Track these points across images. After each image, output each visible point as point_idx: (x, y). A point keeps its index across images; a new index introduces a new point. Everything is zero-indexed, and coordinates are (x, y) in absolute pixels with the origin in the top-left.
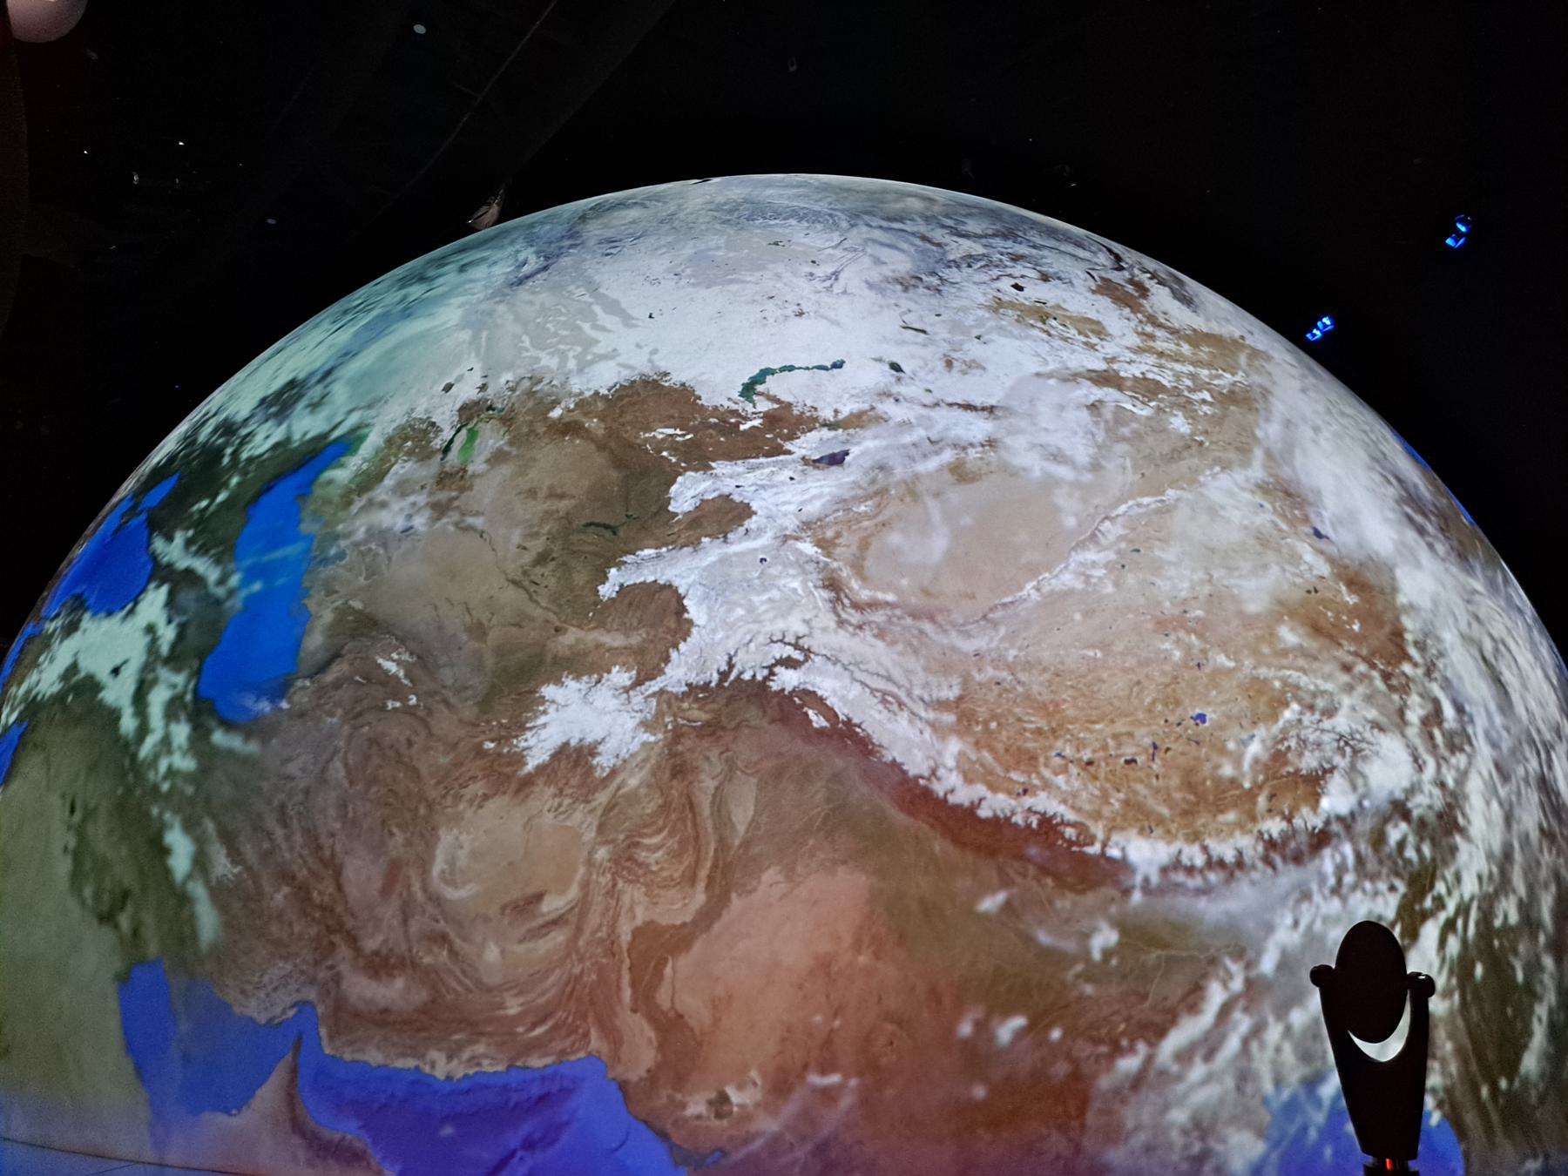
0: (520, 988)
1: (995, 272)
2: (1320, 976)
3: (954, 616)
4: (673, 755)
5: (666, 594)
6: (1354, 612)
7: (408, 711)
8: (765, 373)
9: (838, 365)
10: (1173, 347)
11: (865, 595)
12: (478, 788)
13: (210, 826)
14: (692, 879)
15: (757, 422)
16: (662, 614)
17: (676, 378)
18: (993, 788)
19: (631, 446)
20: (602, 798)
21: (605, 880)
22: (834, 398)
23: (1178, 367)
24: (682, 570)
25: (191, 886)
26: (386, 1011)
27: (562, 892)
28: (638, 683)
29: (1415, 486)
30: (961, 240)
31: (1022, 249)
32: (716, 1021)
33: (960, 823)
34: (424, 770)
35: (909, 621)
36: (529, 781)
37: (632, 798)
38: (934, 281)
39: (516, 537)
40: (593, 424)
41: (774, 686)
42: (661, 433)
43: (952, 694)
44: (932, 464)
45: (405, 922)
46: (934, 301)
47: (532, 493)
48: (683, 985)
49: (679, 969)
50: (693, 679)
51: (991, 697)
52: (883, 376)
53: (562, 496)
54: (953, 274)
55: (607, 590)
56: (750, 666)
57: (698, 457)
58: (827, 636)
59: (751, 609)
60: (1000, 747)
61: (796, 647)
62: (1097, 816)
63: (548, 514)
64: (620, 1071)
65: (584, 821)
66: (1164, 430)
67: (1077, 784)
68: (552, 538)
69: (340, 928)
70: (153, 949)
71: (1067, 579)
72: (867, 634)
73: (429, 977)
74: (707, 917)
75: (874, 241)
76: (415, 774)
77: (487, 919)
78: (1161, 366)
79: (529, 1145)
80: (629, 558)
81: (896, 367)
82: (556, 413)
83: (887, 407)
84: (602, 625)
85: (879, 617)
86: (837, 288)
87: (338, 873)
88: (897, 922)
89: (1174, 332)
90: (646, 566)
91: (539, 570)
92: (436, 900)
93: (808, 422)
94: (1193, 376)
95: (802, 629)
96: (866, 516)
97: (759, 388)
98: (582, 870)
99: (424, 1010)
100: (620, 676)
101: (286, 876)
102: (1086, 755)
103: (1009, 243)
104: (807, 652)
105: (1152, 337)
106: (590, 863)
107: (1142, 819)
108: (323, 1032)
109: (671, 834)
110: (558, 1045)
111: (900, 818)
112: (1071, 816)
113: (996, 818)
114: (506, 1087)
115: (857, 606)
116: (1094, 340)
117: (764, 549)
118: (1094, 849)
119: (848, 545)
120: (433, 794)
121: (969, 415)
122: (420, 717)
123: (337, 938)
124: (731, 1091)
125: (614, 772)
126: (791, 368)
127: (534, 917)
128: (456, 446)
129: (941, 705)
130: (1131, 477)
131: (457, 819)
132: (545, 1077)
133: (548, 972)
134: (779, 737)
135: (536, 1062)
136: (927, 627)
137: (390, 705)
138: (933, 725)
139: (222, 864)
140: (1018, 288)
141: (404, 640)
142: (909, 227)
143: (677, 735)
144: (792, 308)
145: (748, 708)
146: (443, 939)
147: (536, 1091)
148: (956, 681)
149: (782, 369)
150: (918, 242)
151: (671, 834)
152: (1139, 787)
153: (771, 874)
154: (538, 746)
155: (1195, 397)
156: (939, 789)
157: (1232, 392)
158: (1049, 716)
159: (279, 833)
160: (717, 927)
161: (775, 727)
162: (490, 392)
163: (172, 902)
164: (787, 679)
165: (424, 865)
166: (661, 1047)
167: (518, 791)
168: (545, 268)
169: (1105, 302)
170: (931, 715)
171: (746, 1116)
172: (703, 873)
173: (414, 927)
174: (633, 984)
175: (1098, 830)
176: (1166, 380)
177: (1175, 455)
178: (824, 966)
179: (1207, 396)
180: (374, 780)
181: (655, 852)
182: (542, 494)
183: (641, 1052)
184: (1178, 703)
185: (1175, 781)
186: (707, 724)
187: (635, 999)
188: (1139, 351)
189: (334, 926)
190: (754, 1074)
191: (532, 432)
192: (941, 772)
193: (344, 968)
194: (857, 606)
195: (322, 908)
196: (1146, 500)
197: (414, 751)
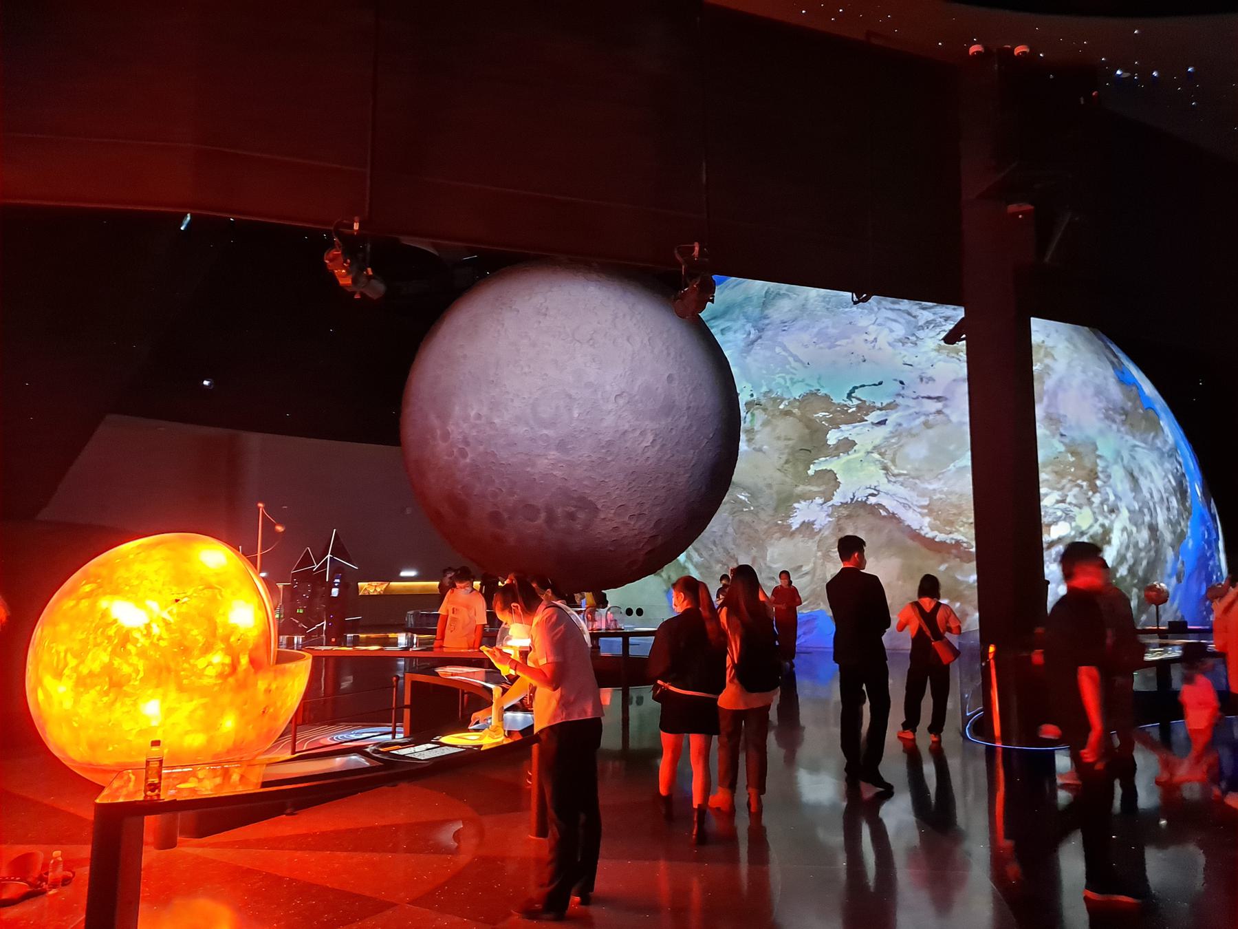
1: (938, 330)
6: (1072, 464)
7: (750, 511)
8: (855, 388)
9: (880, 383)
11: (896, 472)
12: (777, 535)
16: (829, 480)
20: (817, 538)
24: (834, 465)
33: (930, 544)
36: (793, 534)
38: (914, 338)
39: (776, 456)
40: (795, 411)
42: (821, 414)
47: (779, 438)
54: (921, 334)
55: (811, 472)
56: (860, 497)
58: (884, 485)
63: (787, 446)
65: (812, 545)
72: (898, 485)
76: (756, 531)
81: (902, 383)
82: (782, 407)
83: (899, 400)
85: (901, 479)
90: (821, 464)
92: (770, 568)
93: (873, 408)
100: (819, 500)
111: (910, 542)
115: (894, 475)
119: (889, 454)
122: (755, 514)
132: (808, 615)
143: (839, 519)
154: (795, 522)
156: (923, 533)
164: (872, 500)
165: (765, 559)
168: (760, 337)
194: (894, 475)
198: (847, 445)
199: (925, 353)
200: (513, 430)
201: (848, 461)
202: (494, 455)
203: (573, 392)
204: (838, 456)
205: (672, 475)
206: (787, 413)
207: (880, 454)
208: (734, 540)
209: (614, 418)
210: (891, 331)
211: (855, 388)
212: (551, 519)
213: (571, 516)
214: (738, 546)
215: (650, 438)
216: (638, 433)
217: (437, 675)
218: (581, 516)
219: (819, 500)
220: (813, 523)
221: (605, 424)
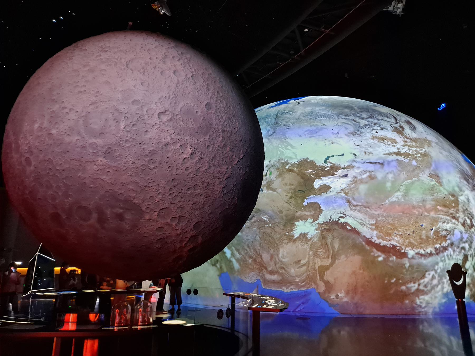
0: (299, 276)
1: (371, 129)
2: (448, 272)
3: (373, 207)
4: (322, 235)
5: (316, 204)
6: (453, 202)
7: (270, 227)
8: (328, 157)
9: (343, 155)
10: (411, 144)
12: (286, 241)
13: (234, 248)
14: (328, 257)
15: (329, 168)
17: (310, 159)
18: (383, 240)
19: (304, 174)
20: (310, 243)
21: (312, 257)
22: (343, 162)
23: (413, 149)
25: (231, 259)
26: (274, 280)
27: (304, 260)
28: (314, 222)
29: (466, 169)
30: (362, 120)
31: (376, 121)
32: (335, 282)
34: (275, 238)
35: (364, 208)
36: (295, 240)
37: (316, 243)
38: (359, 133)
40: (295, 169)
41: (340, 222)
43: (374, 222)
44: (364, 176)
45: (275, 265)
46: (360, 138)
47: (286, 184)
48: (329, 276)
49: (327, 273)
50: (324, 221)
51: (382, 223)
52: (352, 157)
53: (292, 185)
54: (363, 130)
55: (305, 204)
56: (335, 218)
57: (318, 176)
59: (333, 207)
60: (384, 232)
61: (343, 214)
62: (403, 245)
63: (290, 189)
64: (318, 291)
65: (307, 247)
66: (411, 165)
67: (399, 239)
68: (292, 193)
69: (263, 266)
70: (225, 270)
71: (394, 199)
73: (280, 274)
74: (332, 264)
75: (344, 123)
76: (273, 239)
77: (291, 264)
78: (409, 149)
79: (303, 303)
80: (308, 197)
81: (355, 155)
82: (287, 167)
83: (354, 164)
84: (305, 211)
85: (358, 208)
86: (339, 136)
87: (261, 257)
88: (369, 263)
89: (411, 139)
91: (291, 200)
92: (281, 261)
94: (416, 151)
95: (344, 211)
96: (353, 187)
97: (328, 161)
98: (308, 256)
99: (281, 280)
100: (310, 220)
101: (251, 257)
102: (401, 233)
103: (373, 120)
104: (345, 215)
105: (406, 142)
106: (309, 254)
107: (411, 245)
108: (262, 284)
109: (324, 249)
110: (307, 286)
112: (398, 245)
113: (384, 246)
114: (298, 294)
115: (354, 206)
116: (395, 144)
117: (334, 195)
118: (403, 251)
120: (278, 242)
121: (371, 165)
123: (263, 268)
124: (339, 294)
125: (311, 238)
126: (333, 156)
127: (300, 264)
128: (268, 174)
129: (372, 225)
130: (405, 176)
131: (283, 247)
132: (305, 292)
133: (304, 274)
134: (341, 231)
135: (303, 289)
136: (368, 209)
137: (266, 226)
138: (371, 229)
139: (238, 255)
140: (377, 132)
141: (266, 214)
142: (350, 118)
143: (322, 231)
144: (331, 142)
145: (334, 226)
146: (283, 268)
147: (303, 294)
148: (374, 220)
149: (332, 156)
150: (353, 122)
151: (324, 249)
152: (411, 239)
153: (343, 256)
154: (296, 234)
155: (417, 156)
156: (373, 240)
157: (425, 153)
158: (393, 226)
159: (248, 249)
160: (334, 266)
161: (341, 230)
162: (272, 162)
163: (228, 262)
164: (342, 220)
165: (278, 255)
166: (326, 286)
167: (294, 242)
169: (395, 134)
170: (370, 227)
171: (342, 299)
172: (330, 256)
173: (277, 266)
174: (319, 276)
175: (403, 247)
176: (411, 153)
177: (413, 171)
178: (354, 273)
179: (419, 155)
180: (265, 240)
181: (321, 252)
182: (288, 184)
183: (322, 288)
184: (418, 223)
185: (418, 238)
186: (328, 229)
187: (320, 278)
188: (404, 146)
189: (262, 266)
190: (343, 291)
191: (283, 171)
192: (373, 237)
193: (265, 273)
194: (354, 206)
195: (259, 263)
196: (409, 181)
197: (272, 234)
198: (326, 188)
199: (366, 140)
200: (67, 139)
201: (327, 197)
202: (50, 161)
203: (121, 108)
204: (321, 194)
205: (209, 184)
206: (290, 171)
207: (345, 193)
208: (260, 244)
209: (157, 133)
210: (346, 129)
211: (330, 157)
212: (102, 219)
213: (120, 217)
214: (262, 248)
215: (189, 150)
216: (179, 145)
217: (58, 331)
218: (128, 216)
219: (310, 220)
220: (307, 234)
221: (149, 136)
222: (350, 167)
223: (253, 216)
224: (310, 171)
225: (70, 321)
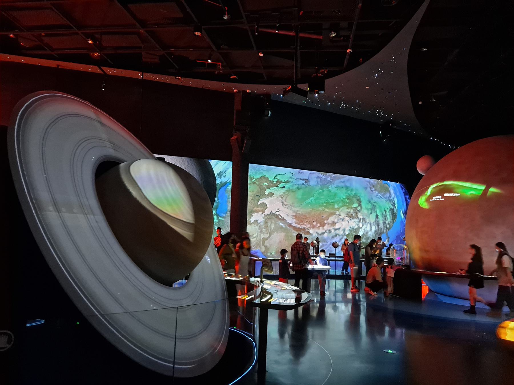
48: (267, 243)
49: (266, 242)
55: (259, 203)
56: (273, 212)
57: (269, 187)
83: (291, 180)
85: (287, 206)
100: (260, 213)
143: (266, 219)
145: (274, 216)
164: (277, 213)
178: (280, 242)
183: (263, 249)
222: (288, 182)
223: (403, 204)
224: (264, 184)
225: (175, 366)
